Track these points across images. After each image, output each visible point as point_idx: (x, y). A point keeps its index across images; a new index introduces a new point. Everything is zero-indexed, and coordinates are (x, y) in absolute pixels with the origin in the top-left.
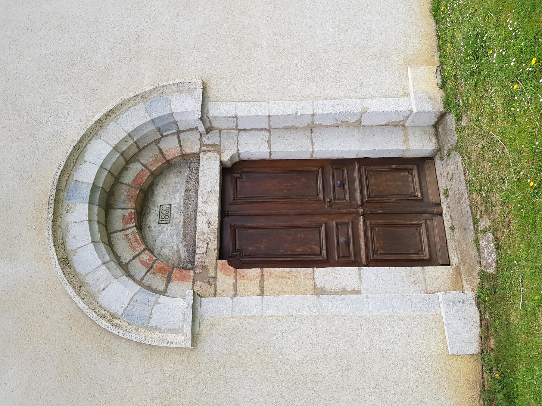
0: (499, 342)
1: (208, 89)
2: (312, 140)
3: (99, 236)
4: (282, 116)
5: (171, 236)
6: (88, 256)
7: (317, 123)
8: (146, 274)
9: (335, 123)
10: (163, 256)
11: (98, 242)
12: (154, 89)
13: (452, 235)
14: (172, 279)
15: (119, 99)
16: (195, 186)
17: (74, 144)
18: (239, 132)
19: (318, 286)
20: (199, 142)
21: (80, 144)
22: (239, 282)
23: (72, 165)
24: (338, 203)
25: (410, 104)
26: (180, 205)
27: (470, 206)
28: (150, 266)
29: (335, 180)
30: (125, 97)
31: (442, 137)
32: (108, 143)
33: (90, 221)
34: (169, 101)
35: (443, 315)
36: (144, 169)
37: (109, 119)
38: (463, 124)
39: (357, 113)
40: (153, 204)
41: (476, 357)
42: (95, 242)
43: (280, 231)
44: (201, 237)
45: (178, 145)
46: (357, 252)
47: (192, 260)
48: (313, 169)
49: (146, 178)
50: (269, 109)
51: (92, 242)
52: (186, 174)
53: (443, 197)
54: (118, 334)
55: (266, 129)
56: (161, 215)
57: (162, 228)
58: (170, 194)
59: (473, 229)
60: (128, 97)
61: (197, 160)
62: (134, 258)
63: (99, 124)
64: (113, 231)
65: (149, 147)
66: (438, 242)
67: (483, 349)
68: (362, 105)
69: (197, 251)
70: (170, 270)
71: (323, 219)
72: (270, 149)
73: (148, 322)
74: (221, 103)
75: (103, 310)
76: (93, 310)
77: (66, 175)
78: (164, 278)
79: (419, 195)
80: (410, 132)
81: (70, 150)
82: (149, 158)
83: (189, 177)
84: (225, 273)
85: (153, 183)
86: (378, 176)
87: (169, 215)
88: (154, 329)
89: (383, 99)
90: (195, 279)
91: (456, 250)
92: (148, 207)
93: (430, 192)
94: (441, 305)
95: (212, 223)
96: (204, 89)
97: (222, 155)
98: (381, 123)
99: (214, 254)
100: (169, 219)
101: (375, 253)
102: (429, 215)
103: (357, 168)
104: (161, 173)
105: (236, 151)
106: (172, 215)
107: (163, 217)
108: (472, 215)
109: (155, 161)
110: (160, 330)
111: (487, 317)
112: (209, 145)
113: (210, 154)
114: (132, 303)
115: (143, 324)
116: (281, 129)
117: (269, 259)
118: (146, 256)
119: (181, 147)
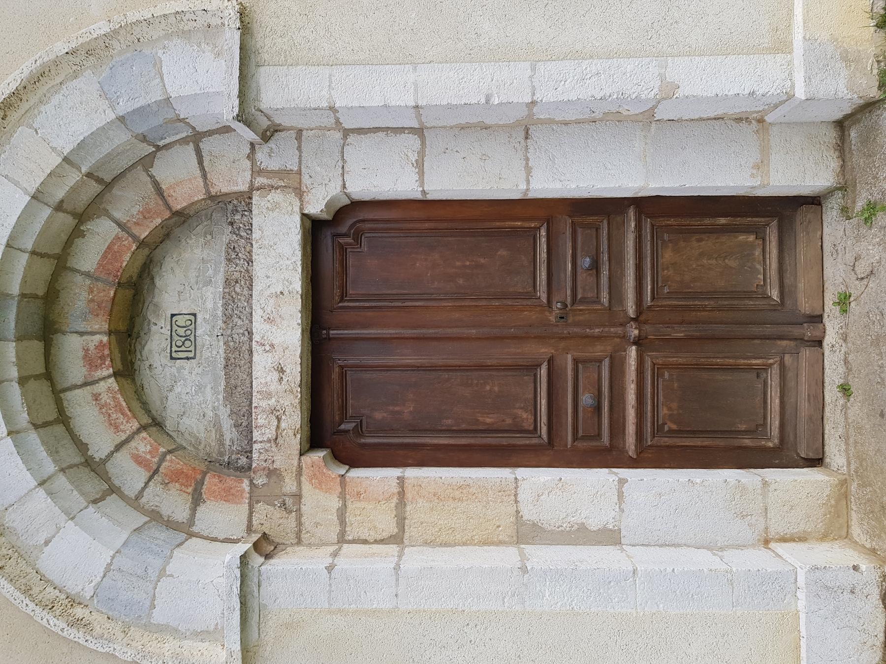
1: (255, 27)
2: (527, 159)
3: (25, 415)
4: (450, 107)
5: (200, 388)
7: (542, 117)
8: (147, 484)
9: (586, 116)
10: (186, 435)
11: (25, 430)
12: (115, 32)
13: (842, 402)
14: (204, 496)
18: (345, 137)
19: (525, 518)
20: (249, 163)
22: (350, 505)
24: (581, 310)
25: (790, 74)
26: (215, 316)
28: (155, 467)
31: (857, 159)
32: (17, 184)
34: (157, 64)
35: (803, 616)
39: (647, 100)
40: (154, 312)
42: (18, 432)
43: (446, 375)
44: (264, 404)
45: (198, 173)
46: (617, 428)
48: (526, 225)
49: (127, 257)
50: (416, 85)
52: (225, 239)
53: (831, 310)
54: (85, 644)
55: (412, 130)
56: (175, 338)
57: (179, 372)
58: (188, 287)
60: (52, 57)
62: (118, 447)
64: (65, 385)
65: (128, 175)
66: (804, 408)
68: (662, 78)
69: (256, 435)
70: (199, 477)
71: (544, 351)
72: (422, 184)
73: (150, 615)
75: (50, 589)
76: (27, 591)
78: (185, 495)
79: (775, 294)
82: (130, 204)
83: (232, 248)
84: (320, 483)
85: (151, 261)
86: (682, 244)
87: (192, 338)
88: (162, 629)
89: (720, 59)
90: (254, 499)
91: (846, 438)
92: (145, 318)
93: (801, 286)
94: (801, 595)
95: (288, 371)
96: (246, 28)
97: (306, 198)
98: (705, 116)
99: (293, 442)
100: (192, 348)
101: (658, 430)
102: (793, 344)
103: (633, 224)
104: (167, 236)
105: (339, 189)
109: (146, 214)
110: (175, 632)
112: (272, 172)
113: (275, 196)
117: (416, 441)
118: (143, 445)
119: (204, 176)
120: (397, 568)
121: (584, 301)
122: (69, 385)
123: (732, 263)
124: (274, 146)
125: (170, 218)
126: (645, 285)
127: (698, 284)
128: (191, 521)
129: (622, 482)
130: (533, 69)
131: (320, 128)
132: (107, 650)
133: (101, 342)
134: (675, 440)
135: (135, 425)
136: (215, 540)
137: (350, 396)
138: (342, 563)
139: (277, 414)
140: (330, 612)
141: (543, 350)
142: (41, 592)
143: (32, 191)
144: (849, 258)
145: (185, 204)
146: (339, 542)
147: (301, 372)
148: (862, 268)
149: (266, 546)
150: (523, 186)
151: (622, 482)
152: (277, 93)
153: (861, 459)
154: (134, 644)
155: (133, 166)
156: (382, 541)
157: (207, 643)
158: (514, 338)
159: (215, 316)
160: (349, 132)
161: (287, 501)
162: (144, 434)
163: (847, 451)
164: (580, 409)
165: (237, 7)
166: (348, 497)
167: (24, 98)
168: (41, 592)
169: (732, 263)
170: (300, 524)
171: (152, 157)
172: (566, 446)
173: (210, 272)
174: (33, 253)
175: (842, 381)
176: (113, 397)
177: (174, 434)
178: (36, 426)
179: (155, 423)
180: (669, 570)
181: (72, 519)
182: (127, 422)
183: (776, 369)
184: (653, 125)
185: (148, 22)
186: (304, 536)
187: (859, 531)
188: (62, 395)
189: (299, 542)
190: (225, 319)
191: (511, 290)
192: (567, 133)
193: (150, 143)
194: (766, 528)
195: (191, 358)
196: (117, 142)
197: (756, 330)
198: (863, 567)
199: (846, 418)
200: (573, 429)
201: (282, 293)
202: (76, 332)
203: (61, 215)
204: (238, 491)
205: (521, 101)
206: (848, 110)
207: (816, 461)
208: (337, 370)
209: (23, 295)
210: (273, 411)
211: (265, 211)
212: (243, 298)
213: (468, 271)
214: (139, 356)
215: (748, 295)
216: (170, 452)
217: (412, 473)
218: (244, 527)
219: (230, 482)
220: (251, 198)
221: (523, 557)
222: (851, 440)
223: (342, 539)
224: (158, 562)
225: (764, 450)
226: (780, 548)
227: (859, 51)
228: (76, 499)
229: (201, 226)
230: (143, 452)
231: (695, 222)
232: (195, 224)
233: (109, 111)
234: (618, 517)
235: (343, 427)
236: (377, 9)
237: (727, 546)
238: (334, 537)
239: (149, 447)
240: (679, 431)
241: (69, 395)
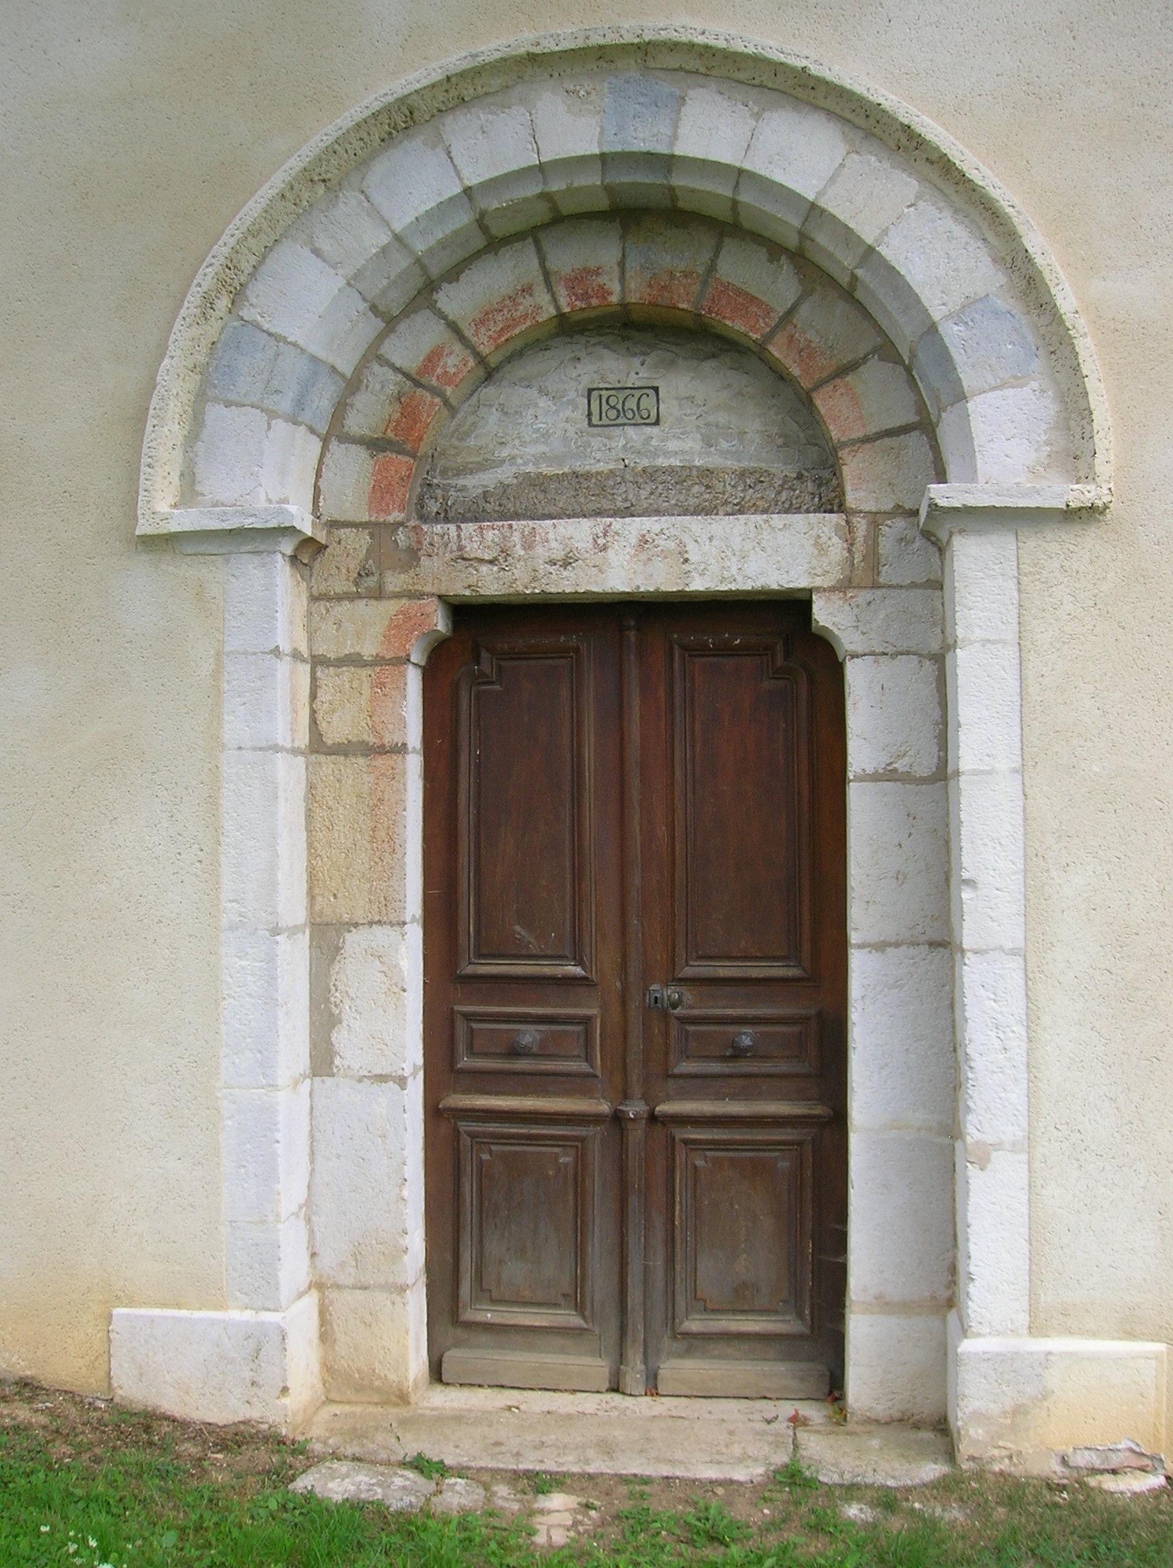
2: (897, 945)
6: (418, 190)
8: (398, 370)
16: (726, 503)
17: (814, 70)
19: (347, 936)
23: (742, 76)
28: (423, 381)
32: (833, 180)
33: (541, 168)
34: (1017, 381)
44: (516, 538)
45: (872, 429)
47: (450, 515)
50: (989, 773)
56: (622, 395)
57: (570, 402)
58: (694, 418)
60: (1021, 230)
61: (830, 502)
62: (453, 327)
68: (998, 1146)
69: (469, 528)
70: (409, 447)
73: (216, 400)
74: (1012, 585)
75: (253, 260)
76: (253, 233)
82: (821, 324)
84: (396, 628)
94: (248, 1315)
95: (565, 573)
97: (836, 597)
99: (459, 588)
100: (605, 421)
106: (618, 431)
107: (613, 401)
109: (806, 353)
112: (876, 544)
113: (837, 549)
114: (273, 343)
115: (211, 386)
120: (276, 749)
128: (346, 439)
129: (402, 1082)
130: (1013, 952)
132: (171, 347)
135: (485, 350)
136: (318, 475)
138: (283, 668)
140: (219, 654)
142: (250, 250)
143: (822, 203)
147: (564, 593)
149: (307, 552)
156: (314, 721)
157: (178, 483)
159: (655, 455)
161: (371, 578)
162: (472, 363)
165: (1099, 503)
166: (378, 669)
168: (250, 250)
170: (339, 598)
176: (527, 315)
177: (474, 399)
179: (489, 373)
181: (349, 284)
182: (490, 337)
186: (322, 606)
189: (314, 599)
190: (650, 470)
192: (937, 1008)
195: (590, 420)
198: (286, 1401)
201: (686, 560)
202: (624, 255)
204: (387, 505)
207: (437, 1373)
209: (672, 189)
210: (506, 552)
214: (593, 341)
216: (446, 402)
217: (414, 765)
218: (337, 517)
221: (294, 931)
223: (318, 661)
226: (310, 1303)
230: (445, 364)
238: (321, 650)
239: (453, 370)
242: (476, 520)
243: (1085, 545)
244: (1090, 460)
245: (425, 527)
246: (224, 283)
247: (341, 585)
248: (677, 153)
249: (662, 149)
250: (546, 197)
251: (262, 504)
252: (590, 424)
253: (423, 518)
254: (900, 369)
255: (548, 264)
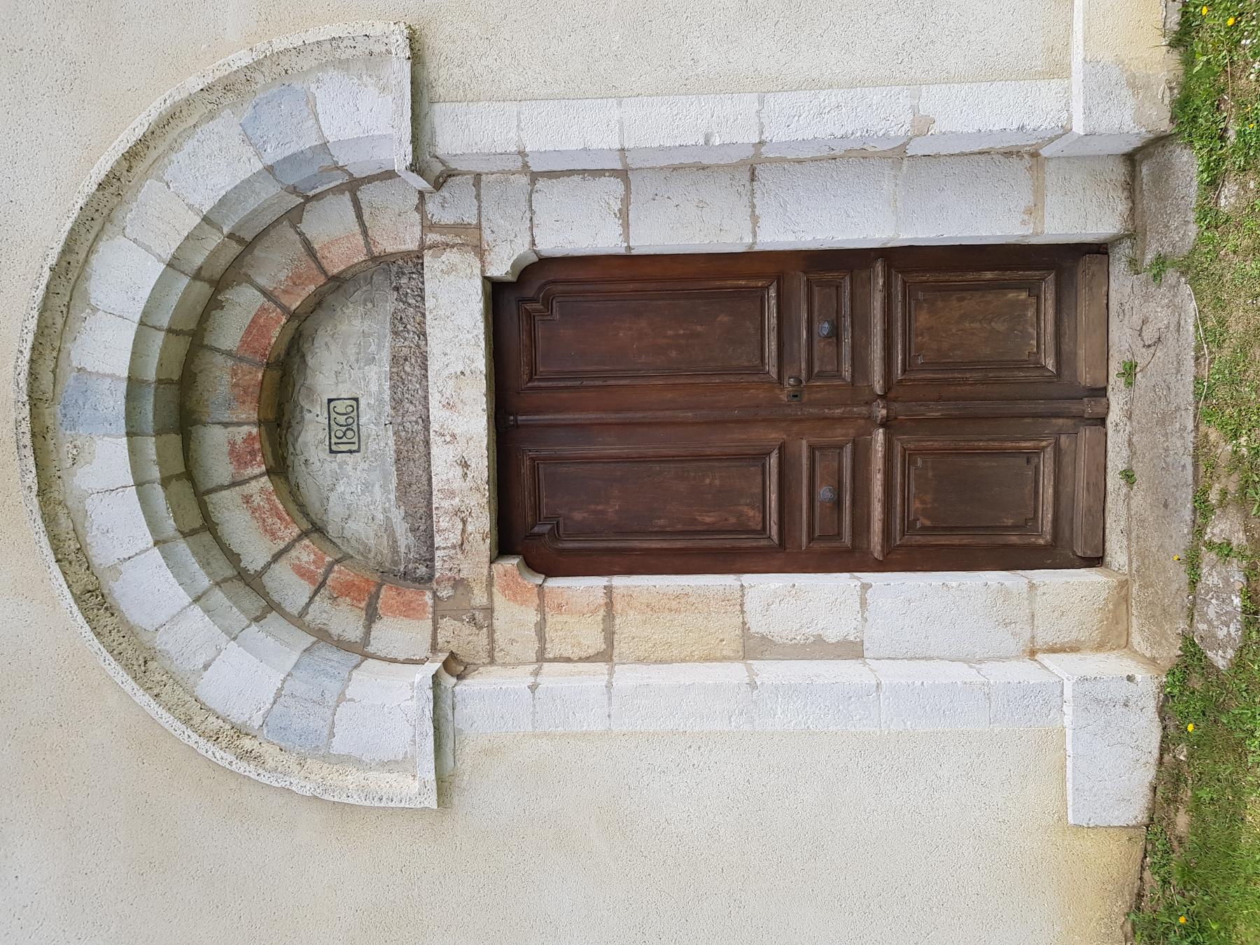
0: (1200, 824)
2: (753, 206)
4: (661, 149)
5: (367, 486)
6: (154, 585)
10: (353, 542)
11: (173, 539)
12: (259, 63)
13: (1124, 490)
15: (156, 104)
16: (418, 346)
17: (52, 260)
19: (752, 630)
20: (418, 216)
21: (68, 258)
23: (59, 321)
25: (1067, 103)
26: (381, 401)
27: (1196, 457)
28: (320, 580)
29: (816, 319)
30: (173, 94)
31: (1148, 203)
32: (148, 249)
33: (139, 485)
34: (310, 101)
35: (1069, 733)
36: (268, 304)
37: (140, 167)
38: (1223, 202)
40: (308, 396)
41: (1132, 832)
42: (165, 542)
43: (657, 467)
44: (446, 504)
45: (357, 229)
48: (753, 284)
49: (276, 332)
50: (621, 124)
51: (155, 544)
55: (614, 173)
56: (335, 427)
57: (340, 467)
58: (349, 366)
59: (1189, 522)
60: (184, 95)
61: (416, 265)
62: (276, 557)
63: (112, 190)
65: (272, 233)
66: (1083, 499)
67: (1156, 822)
68: (915, 110)
69: (438, 540)
70: (373, 590)
71: (774, 436)
72: (627, 239)
73: (329, 745)
74: (474, 107)
75: (212, 719)
76: (188, 721)
77: (49, 355)
78: (358, 611)
79: (1050, 363)
80: (1051, 176)
81: (44, 281)
82: (275, 267)
83: (398, 319)
84: (515, 594)
85: (300, 335)
86: (940, 304)
87: (355, 428)
89: (983, 86)
91: (1127, 532)
92: (296, 404)
93: (1081, 353)
95: (473, 465)
96: (416, 58)
97: (488, 258)
99: (483, 547)
100: (355, 439)
101: (908, 527)
102: (1069, 422)
103: (881, 282)
104: (319, 304)
105: (527, 246)
107: (340, 434)
108: (1196, 481)
109: (296, 281)
111: (1182, 758)
112: (446, 226)
113: (451, 256)
114: (282, 699)
115: (317, 749)
116: (662, 169)
118: (305, 554)
119: (365, 232)
120: (609, 686)
121: (821, 375)
122: (214, 485)
123: (1000, 326)
124: (447, 195)
125: (325, 284)
126: (894, 355)
127: (959, 353)
129: (865, 587)
130: (761, 102)
131: (503, 172)
132: (283, 784)
133: (250, 433)
134: (930, 538)
135: (296, 531)
136: (394, 661)
137: (543, 494)
138: (545, 681)
139: (462, 516)
141: (772, 436)
143: (167, 257)
144: (1136, 320)
145: (343, 267)
146: (538, 661)
147: (488, 467)
148: (1149, 334)
149: (455, 666)
150: (748, 240)
151: (865, 587)
152: (455, 137)
153: (1143, 555)
154: (312, 776)
155: (278, 221)
158: (738, 421)
159: (381, 401)
160: (537, 176)
162: (306, 542)
163: (1129, 547)
164: (817, 504)
165: (406, 31)
166: (547, 609)
167: (152, 146)
169: (1000, 326)
170: (492, 641)
171: (300, 209)
172: (801, 547)
173: (373, 348)
174: (170, 331)
175: (1125, 466)
177: (338, 541)
178: (185, 535)
179: (316, 529)
180: (918, 683)
181: (234, 639)
183: (1049, 453)
184: (905, 162)
185: (298, 51)
187: (1139, 639)
188: (206, 498)
189: (492, 661)
191: (734, 363)
193: (298, 194)
194: (1033, 637)
196: (264, 196)
197: (1026, 407)
198: (1139, 678)
199: (1129, 510)
200: (809, 527)
203: (199, 283)
205: (746, 141)
206: (1137, 143)
207: (1096, 560)
208: (528, 463)
209: (159, 381)
210: (458, 511)
211: (439, 274)
212: (414, 379)
213: (682, 342)
214: (291, 450)
215: (1019, 365)
216: (337, 561)
217: (619, 582)
218: (428, 645)
219: (410, 594)
220: (422, 257)
222: (1134, 534)
223: (541, 658)
224: (333, 687)
225: (1034, 548)
227: (1148, 76)
228: (237, 618)
229: (359, 292)
231: (952, 276)
232: (352, 290)
233: (254, 160)
234: (860, 628)
235: (536, 529)
236: (574, 30)
237: (987, 659)
238: (532, 656)
239: (312, 556)
240: (934, 528)
241: (215, 497)
242: (432, 537)
243: (438, 44)
244: (372, 40)
245: (437, 575)
246: (230, 743)
247: (482, 639)
248: (126, 375)
249: (123, 386)
250: (165, 482)
251: (414, 703)
252: (358, 451)
253: (431, 578)
254: (308, 206)
255: (226, 483)
